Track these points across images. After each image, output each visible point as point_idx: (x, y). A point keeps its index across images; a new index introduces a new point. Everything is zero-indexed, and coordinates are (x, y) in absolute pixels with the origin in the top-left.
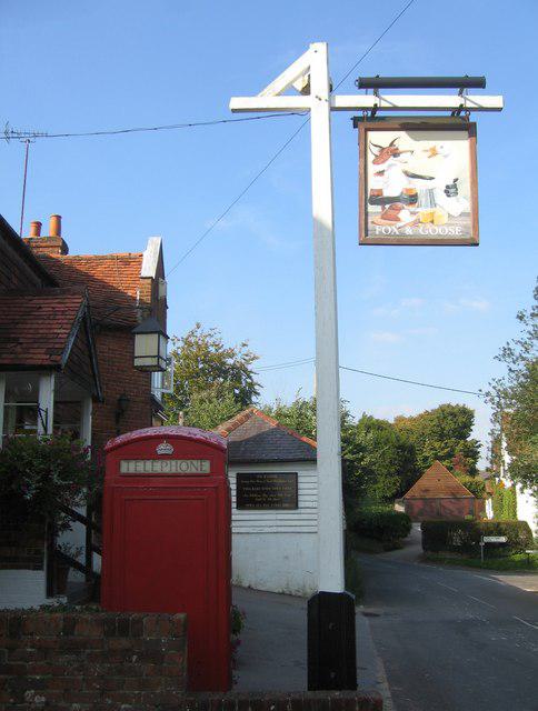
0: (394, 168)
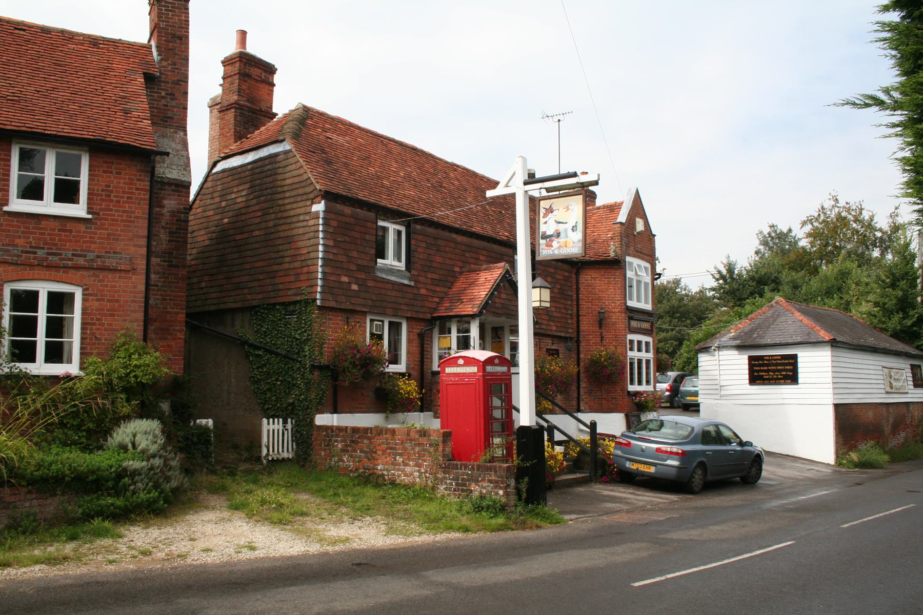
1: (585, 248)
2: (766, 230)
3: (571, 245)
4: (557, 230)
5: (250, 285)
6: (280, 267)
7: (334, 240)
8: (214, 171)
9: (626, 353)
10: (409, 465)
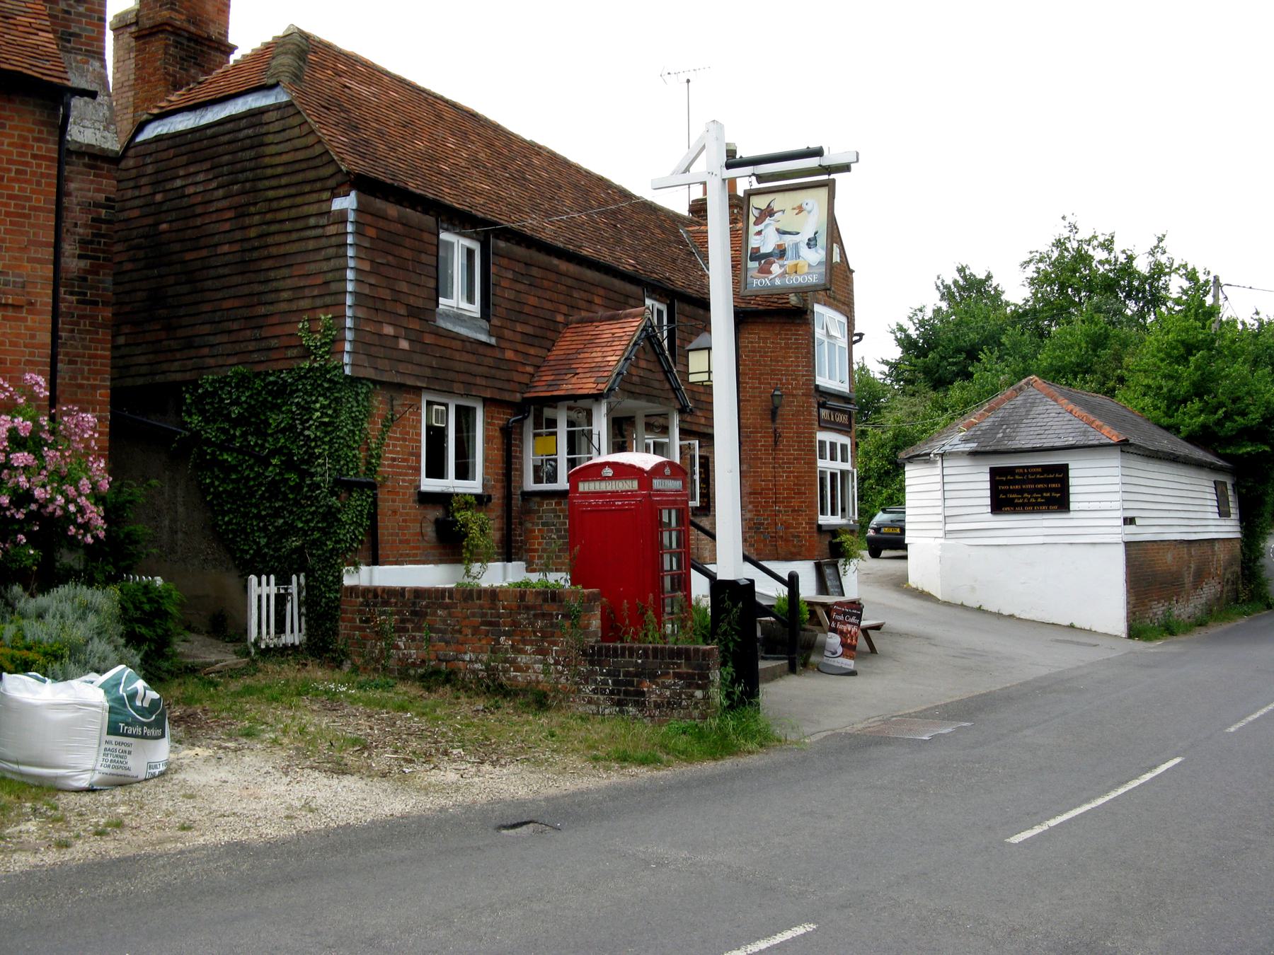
0: (770, 226)
1: (831, 275)
2: (951, 276)
3: (806, 269)
4: (779, 246)
5: (212, 340)
6: (271, 309)
7: (372, 261)
8: (140, 138)
9: (815, 462)
10: (525, 652)
